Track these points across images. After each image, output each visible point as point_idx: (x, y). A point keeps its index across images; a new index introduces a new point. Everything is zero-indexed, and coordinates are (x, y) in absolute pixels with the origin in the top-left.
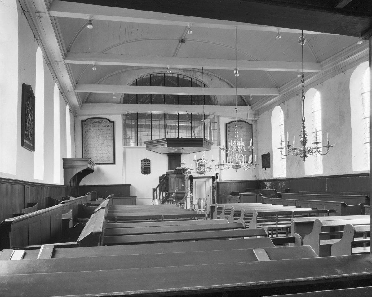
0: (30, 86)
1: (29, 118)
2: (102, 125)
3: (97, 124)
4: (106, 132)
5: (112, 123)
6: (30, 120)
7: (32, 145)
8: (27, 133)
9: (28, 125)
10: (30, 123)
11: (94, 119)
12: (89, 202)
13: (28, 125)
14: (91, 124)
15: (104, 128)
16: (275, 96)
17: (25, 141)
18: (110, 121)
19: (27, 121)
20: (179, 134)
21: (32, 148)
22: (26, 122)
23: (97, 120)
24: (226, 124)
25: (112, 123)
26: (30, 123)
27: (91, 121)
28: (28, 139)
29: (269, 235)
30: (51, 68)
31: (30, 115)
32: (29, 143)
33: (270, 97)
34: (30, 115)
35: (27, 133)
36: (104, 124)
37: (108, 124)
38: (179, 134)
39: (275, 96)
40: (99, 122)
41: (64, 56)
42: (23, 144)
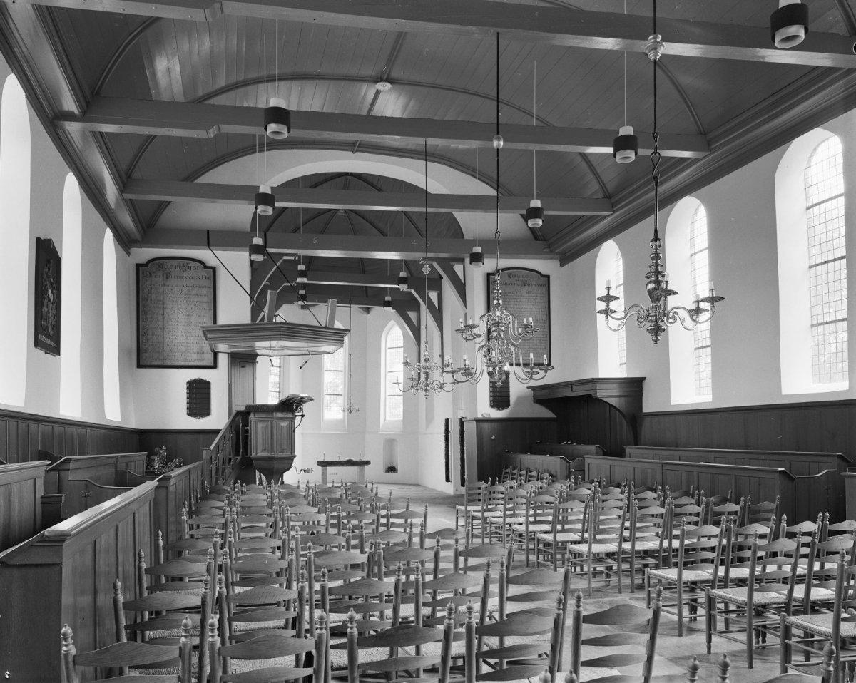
0: (50, 240)
1: (48, 297)
2: (185, 274)
3: (176, 272)
4: (196, 291)
5: (212, 364)
6: (49, 300)
7: (54, 345)
8: (45, 324)
9: (46, 309)
10: (51, 305)
11: (167, 260)
12: (696, 501)
13: (46, 309)
14: (160, 273)
15: (192, 282)
16: (605, 217)
17: (41, 337)
18: (205, 266)
19: (45, 304)
20: (655, 14)
21: (56, 350)
22: (43, 305)
23: (175, 262)
24: (489, 275)
25: (212, 364)
26: (51, 305)
27: (160, 266)
28: (47, 335)
29: (626, 522)
30: (28, 84)
31: (50, 291)
32: (48, 341)
33: (595, 220)
34: (50, 291)
35: (45, 324)
36: (193, 273)
37: (202, 272)
38: (655, 14)
39: (605, 217)
40: (178, 267)
41: (84, 104)
42: (37, 344)
